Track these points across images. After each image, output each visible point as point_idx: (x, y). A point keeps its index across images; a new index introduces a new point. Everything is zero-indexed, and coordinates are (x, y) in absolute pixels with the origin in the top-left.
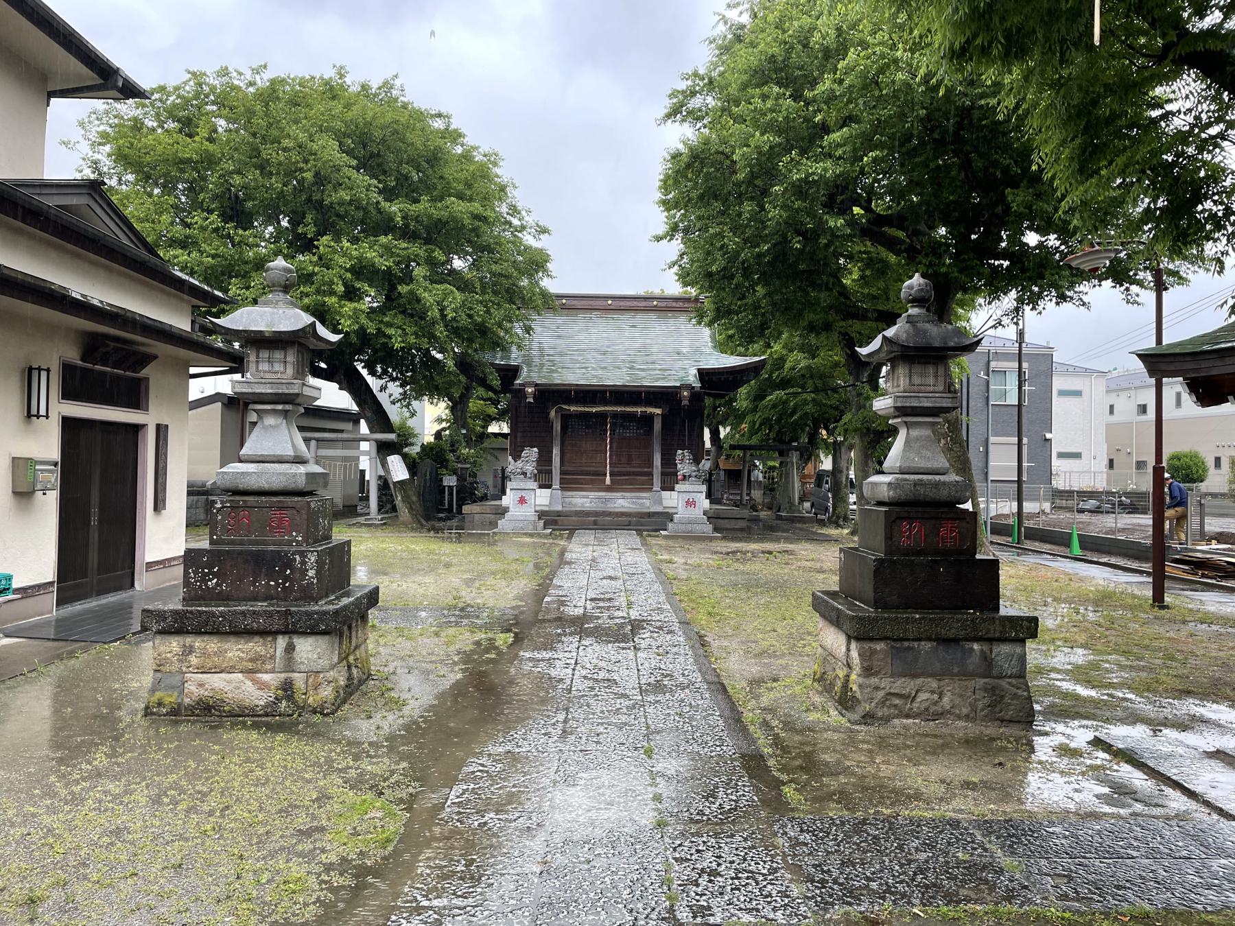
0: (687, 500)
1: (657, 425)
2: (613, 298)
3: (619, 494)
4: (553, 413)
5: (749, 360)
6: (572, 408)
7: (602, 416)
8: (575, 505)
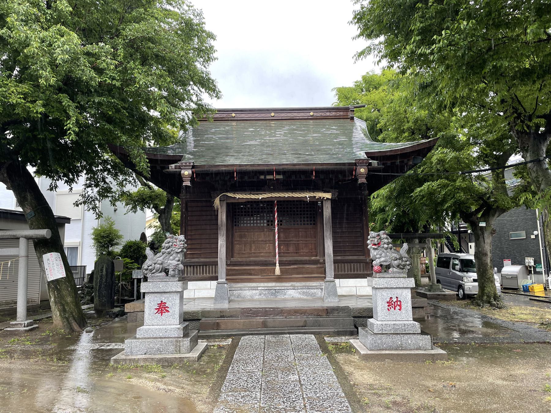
0: (384, 294)
1: (327, 211)
4: (217, 201)
5: (305, 297)
6: (238, 196)
7: (269, 203)
8: (244, 300)
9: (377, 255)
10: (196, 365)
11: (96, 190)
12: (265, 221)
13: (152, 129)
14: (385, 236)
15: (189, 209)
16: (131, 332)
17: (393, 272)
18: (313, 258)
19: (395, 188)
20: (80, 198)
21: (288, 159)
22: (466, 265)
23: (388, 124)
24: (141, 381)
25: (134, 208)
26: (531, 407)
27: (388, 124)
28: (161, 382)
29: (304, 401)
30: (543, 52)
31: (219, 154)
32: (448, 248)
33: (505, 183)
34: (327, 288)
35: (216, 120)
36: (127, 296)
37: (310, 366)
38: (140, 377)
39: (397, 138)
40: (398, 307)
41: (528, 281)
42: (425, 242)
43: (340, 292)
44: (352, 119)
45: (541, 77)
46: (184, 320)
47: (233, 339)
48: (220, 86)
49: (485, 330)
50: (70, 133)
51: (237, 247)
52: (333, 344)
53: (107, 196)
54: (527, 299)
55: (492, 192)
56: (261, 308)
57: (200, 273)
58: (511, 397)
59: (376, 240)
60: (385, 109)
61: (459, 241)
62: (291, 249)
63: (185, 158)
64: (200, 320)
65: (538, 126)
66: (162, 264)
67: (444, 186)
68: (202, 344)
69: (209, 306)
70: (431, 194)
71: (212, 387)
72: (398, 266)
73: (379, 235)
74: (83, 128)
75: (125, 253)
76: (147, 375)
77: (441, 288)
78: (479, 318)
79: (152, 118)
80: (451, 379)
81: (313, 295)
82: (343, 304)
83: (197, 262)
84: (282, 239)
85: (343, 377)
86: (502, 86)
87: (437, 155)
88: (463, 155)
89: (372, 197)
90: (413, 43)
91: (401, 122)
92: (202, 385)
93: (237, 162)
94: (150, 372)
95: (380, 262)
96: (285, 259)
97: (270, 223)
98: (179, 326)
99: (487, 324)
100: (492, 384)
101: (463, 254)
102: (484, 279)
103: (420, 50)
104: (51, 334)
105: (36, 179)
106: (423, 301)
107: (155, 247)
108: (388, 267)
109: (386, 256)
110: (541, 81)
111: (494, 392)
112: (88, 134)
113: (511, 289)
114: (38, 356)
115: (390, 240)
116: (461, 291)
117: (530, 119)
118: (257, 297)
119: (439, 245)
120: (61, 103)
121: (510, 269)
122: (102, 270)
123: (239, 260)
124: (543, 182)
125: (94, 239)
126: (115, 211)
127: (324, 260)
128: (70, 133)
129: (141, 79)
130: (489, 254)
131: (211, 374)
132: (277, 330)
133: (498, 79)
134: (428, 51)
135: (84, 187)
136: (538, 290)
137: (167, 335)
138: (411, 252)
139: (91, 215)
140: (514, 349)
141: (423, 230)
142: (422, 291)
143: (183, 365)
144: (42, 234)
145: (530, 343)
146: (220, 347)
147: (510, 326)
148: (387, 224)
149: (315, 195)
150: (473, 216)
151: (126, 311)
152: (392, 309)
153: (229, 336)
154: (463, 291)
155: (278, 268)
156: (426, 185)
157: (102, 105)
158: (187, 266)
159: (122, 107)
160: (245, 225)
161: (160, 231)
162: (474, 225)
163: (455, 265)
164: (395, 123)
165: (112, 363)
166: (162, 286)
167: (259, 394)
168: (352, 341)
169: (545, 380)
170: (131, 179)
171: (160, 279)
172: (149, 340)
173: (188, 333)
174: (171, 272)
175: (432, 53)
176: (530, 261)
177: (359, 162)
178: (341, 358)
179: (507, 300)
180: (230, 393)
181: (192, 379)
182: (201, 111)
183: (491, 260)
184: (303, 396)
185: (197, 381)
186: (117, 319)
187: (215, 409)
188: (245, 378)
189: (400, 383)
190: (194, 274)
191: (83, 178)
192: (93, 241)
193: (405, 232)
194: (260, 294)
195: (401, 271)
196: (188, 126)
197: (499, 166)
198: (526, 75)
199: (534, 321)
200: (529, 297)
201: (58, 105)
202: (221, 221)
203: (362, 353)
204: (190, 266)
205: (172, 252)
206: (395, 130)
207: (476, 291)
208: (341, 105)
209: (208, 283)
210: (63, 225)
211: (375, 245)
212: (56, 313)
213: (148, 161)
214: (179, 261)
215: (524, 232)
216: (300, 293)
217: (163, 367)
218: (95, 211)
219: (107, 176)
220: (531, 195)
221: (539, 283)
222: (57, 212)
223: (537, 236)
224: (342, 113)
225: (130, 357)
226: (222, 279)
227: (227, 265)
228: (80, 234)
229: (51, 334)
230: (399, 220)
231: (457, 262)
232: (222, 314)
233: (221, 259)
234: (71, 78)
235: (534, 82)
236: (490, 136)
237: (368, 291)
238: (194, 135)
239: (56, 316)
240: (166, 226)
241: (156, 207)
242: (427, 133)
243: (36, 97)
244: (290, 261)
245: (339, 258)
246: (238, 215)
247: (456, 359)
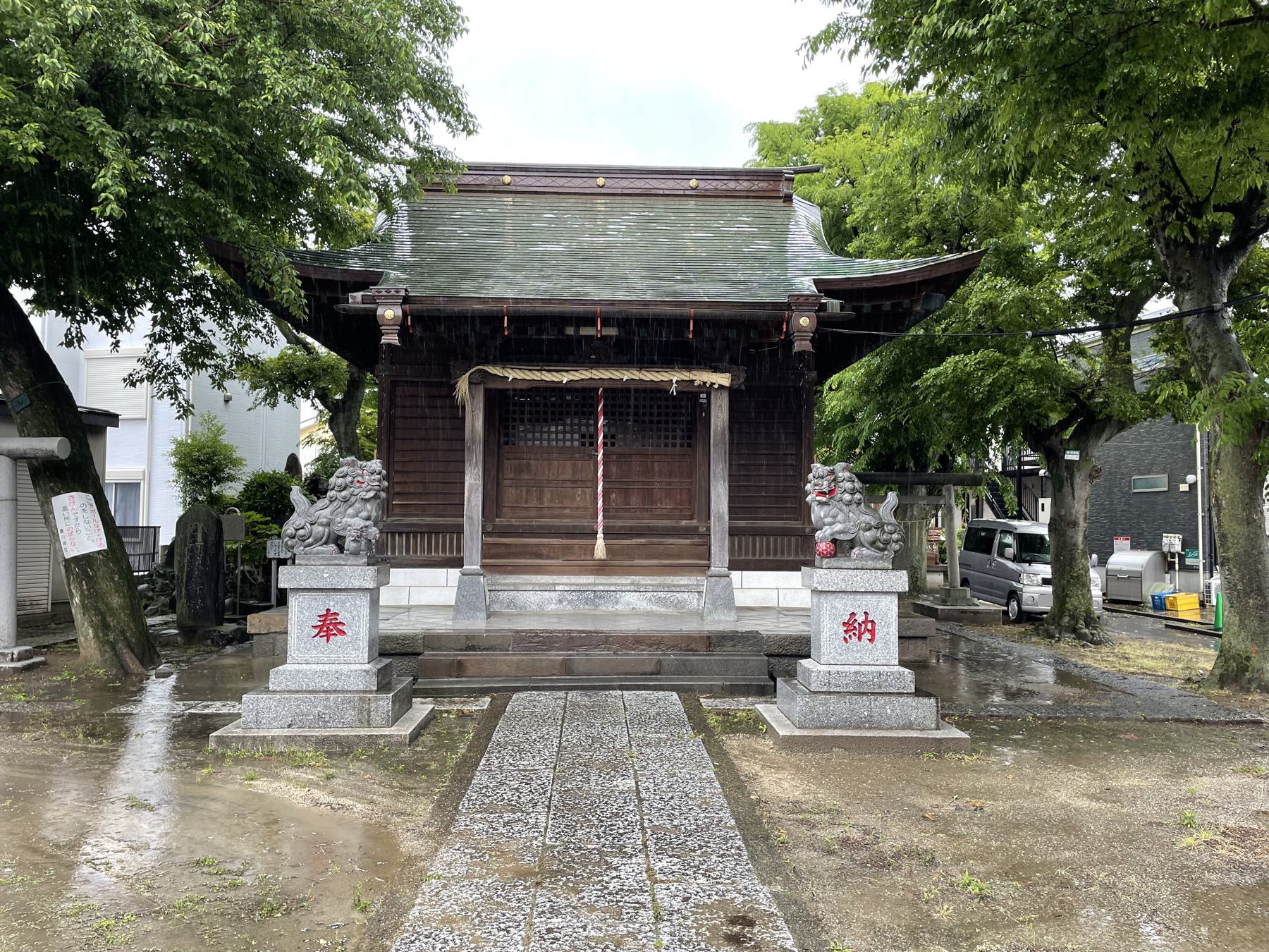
0: (837, 606)
1: (720, 415)
2: (607, 172)
3: (627, 580)
4: (463, 385)
5: (663, 609)
6: (512, 374)
7: (583, 396)
8: (523, 612)
9: (825, 517)
10: (406, 753)
11: (177, 349)
12: (576, 436)
13: (308, 205)
14: (847, 474)
16: (257, 678)
17: (861, 557)
18: (684, 523)
19: (879, 367)
20: (139, 366)
21: (632, 289)
22: (1030, 548)
23: (871, 216)
24: (276, 784)
26: (1149, 860)
27: (871, 216)
28: (324, 788)
29: (644, 835)
30: (1239, 48)
31: (468, 271)
32: (993, 509)
33: (1129, 361)
34: (711, 590)
35: (465, 189)
36: (255, 597)
37: (662, 759)
38: (276, 777)
39: (891, 249)
40: (867, 636)
41: (1164, 586)
42: (940, 494)
43: (741, 599)
44: (788, 198)
45: (1232, 109)
46: (381, 655)
47: (493, 698)
48: (472, 104)
49: (1060, 689)
50: (107, 198)
51: (510, 494)
52: (718, 714)
53: (204, 366)
54: (1160, 625)
55: (1099, 381)
56: (559, 632)
57: (423, 550)
58: (1107, 837)
60: (866, 180)
61: (1019, 494)
62: (635, 501)
63: (387, 280)
65: (1216, 231)
66: (328, 525)
67: (996, 365)
68: (422, 709)
69: (442, 624)
70: (961, 382)
71: (438, 801)
72: (873, 544)
73: (832, 472)
74: (138, 197)
75: (248, 499)
76: (292, 773)
77: (969, 596)
78: (1048, 664)
79: (308, 179)
80: (975, 793)
81: (679, 604)
82: (746, 626)
84: (613, 478)
85: (734, 783)
86: (1140, 126)
87: (981, 290)
88: (1037, 293)
89: (826, 387)
90: (939, 11)
91: (903, 211)
92: (417, 795)
93: (511, 293)
94: (299, 767)
95: (832, 534)
96: (619, 523)
97: (587, 441)
98: (367, 667)
99: (1064, 677)
100: (1064, 806)
101: (1023, 523)
102: (1067, 580)
103: (953, 29)
104: (74, 679)
105: (36, 321)
106: (926, 625)
107: (316, 488)
108: (852, 543)
109: (847, 520)
110: (1229, 120)
111: (1068, 825)
112: (153, 212)
113: (1125, 602)
114: (40, 728)
115: (858, 485)
116: (1014, 604)
117: (1198, 209)
118: (553, 607)
119: (973, 502)
120: (82, 129)
121: (1126, 558)
122: (194, 537)
123: (514, 522)
124: (1216, 362)
125: (176, 465)
126: (227, 401)
127: (709, 529)
128: (107, 198)
129: (279, 81)
130: (1082, 524)
131: (439, 773)
132: (595, 680)
133: (1131, 109)
134: (972, 32)
135: (148, 341)
136: (1186, 607)
137: (340, 685)
138: (909, 514)
139: (166, 408)
140: (1121, 732)
141: (938, 465)
142: (927, 603)
143: (379, 754)
144: (49, 448)
145: (1159, 721)
146: (462, 715)
147: (1116, 682)
148: (858, 451)
149: (693, 377)
150: (1053, 437)
151: (250, 630)
152: (855, 639)
153: (483, 692)
154: (1019, 605)
155: (600, 542)
157: (186, 139)
158: (393, 534)
159: (234, 148)
160: (530, 443)
161: (334, 452)
162: (1053, 457)
163: (1003, 546)
164: (888, 215)
165: (212, 745)
166: (327, 576)
167: (543, 819)
168: (760, 707)
169: (1185, 801)
170: (260, 325)
172: (297, 696)
173: (390, 683)
174: (349, 544)
175: (980, 37)
176: (1173, 542)
177: (798, 303)
178: (733, 743)
179: (1114, 626)
180: (479, 816)
181: (395, 784)
182: (430, 170)
183: (1085, 538)
184: (642, 824)
185: (405, 789)
186: (229, 649)
187: (443, 849)
188: (515, 784)
189: (861, 799)
190: (408, 551)
191: (144, 320)
192: (174, 470)
193: (897, 470)
194: (560, 601)
195: (878, 554)
196: (397, 202)
197: (1119, 320)
198: (1193, 106)
199: (1170, 673)
200: (1164, 622)
201: (78, 136)
203: (782, 732)
204: (400, 534)
205: (353, 499)
206: (886, 230)
207: (1046, 606)
208: (766, 165)
209: (441, 572)
210: (100, 431)
211: (822, 493)
212: (85, 632)
214: (368, 519)
215: (1166, 476)
216: (650, 600)
217: (330, 755)
218: (176, 399)
219: (201, 316)
220: (1185, 387)
221: (1189, 591)
222: (86, 398)
223: (1193, 486)
224: (763, 185)
225: (255, 733)
226: (473, 565)
227: (485, 533)
228: (145, 454)
229: (74, 679)
230: (885, 441)
231: (1009, 539)
232: (471, 643)
233: (471, 518)
234: (110, 70)
235: (1215, 122)
236: (1104, 250)
237: (803, 599)
238: (411, 226)
239: (86, 637)
240: (347, 443)
241: (323, 396)
242: (961, 239)
243: (25, 114)
244: (631, 528)
245: (742, 524)
247: (989, 751)
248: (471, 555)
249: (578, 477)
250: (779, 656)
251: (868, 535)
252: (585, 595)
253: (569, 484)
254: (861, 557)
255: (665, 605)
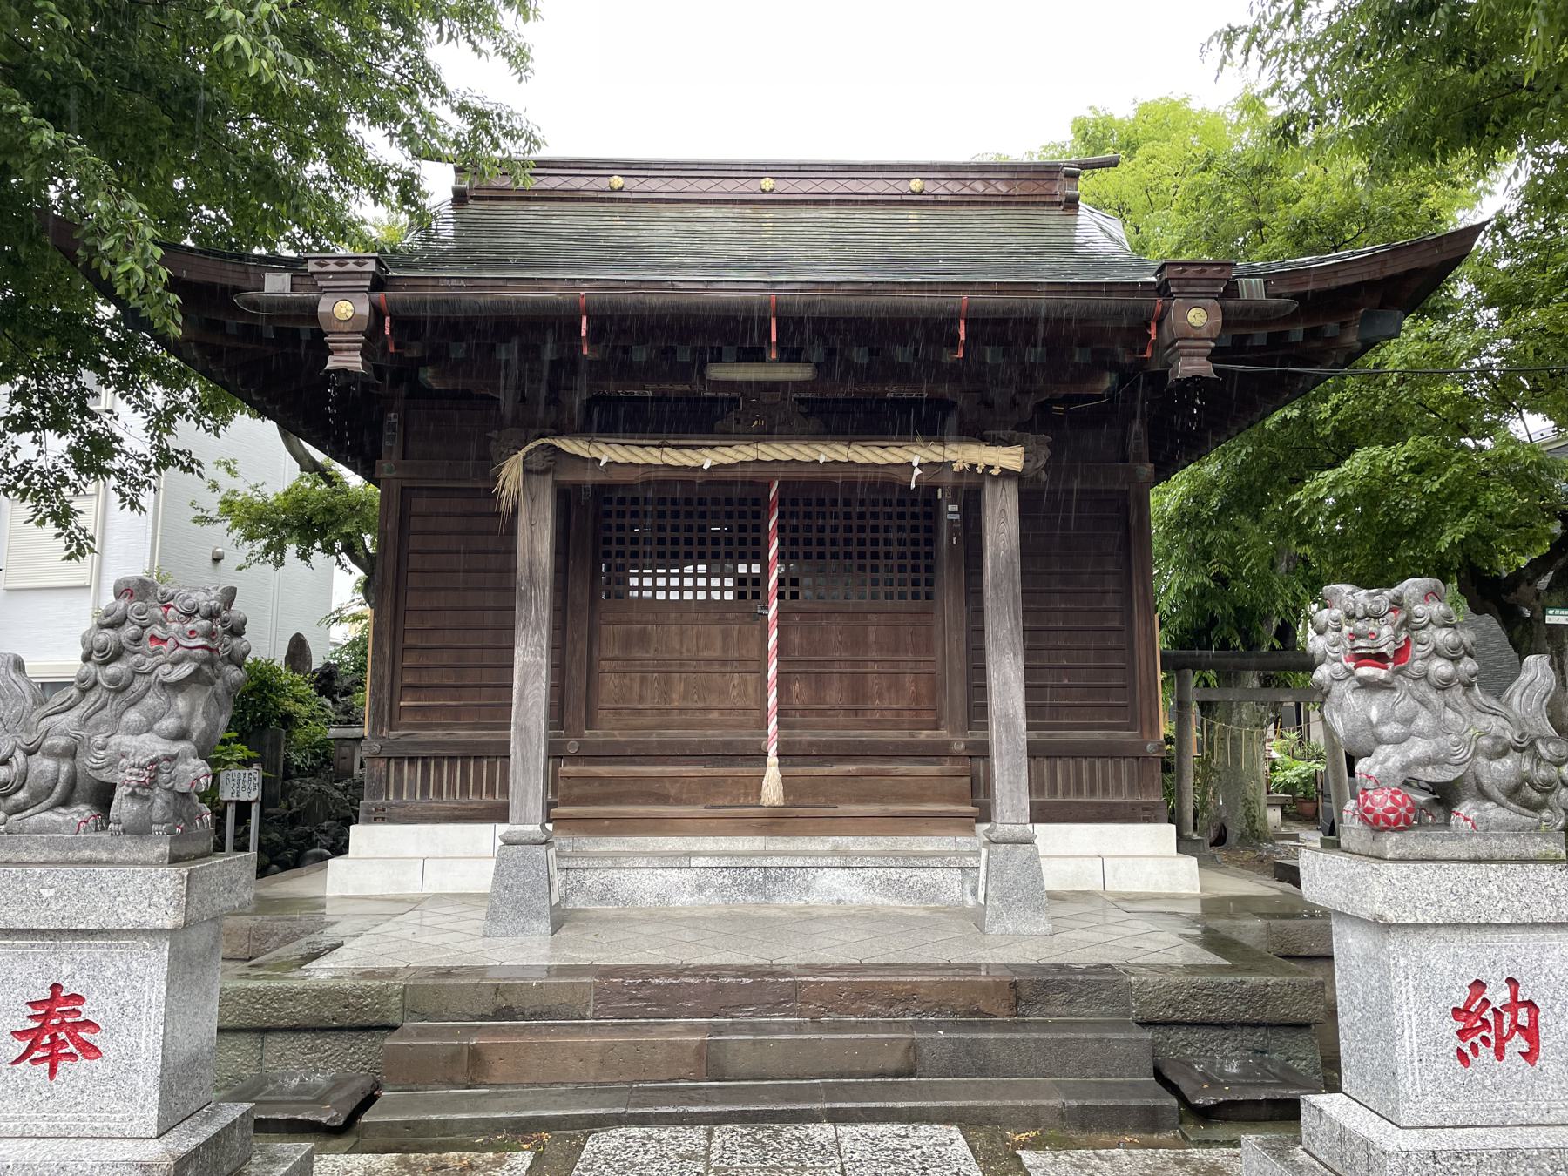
1: (1002, 528)
4: (511, 473)
8: (627, 917)
12: (729, 582)
15: (416, 524)
17: (1483, 829)
18: (924, 735)
25: (275, 550)
40: (1519, 1044)
44: (1072, 203)
57: (451, 790)
59: (1386, 631)
64: (394, 1028)
66: (70, 753)
72: (1513, 792)
73: (1397, 604)
83: (437, 744)
84: (796, 655)
95: (1405, 768)
108: (1445, 797)
109: (1442, 729)
138: (1235, 719)
149: (950, 456)
150: (1523, 587)
152: (1487, 1054)
155: (772, 772)
156: (1357, 463)
171: (54, 844)
190: (425, 792)
194: (700, 888)
195: (1528, 819)
202: (531, 563)
204: (412, 760)
205: (139, 684)
213: (159, 253)
214: (181, 735)
216: (871, 885)
232: (506, 1003)
233: (524, 730)
246: (620, 554)
248: (523, 806)
249: (733, 654)
250: (1167, 1024)
251: (1505, 768)
252: (746, 874)
253: (716, 668)
254: (1483, 829)
255: (899, 894)
